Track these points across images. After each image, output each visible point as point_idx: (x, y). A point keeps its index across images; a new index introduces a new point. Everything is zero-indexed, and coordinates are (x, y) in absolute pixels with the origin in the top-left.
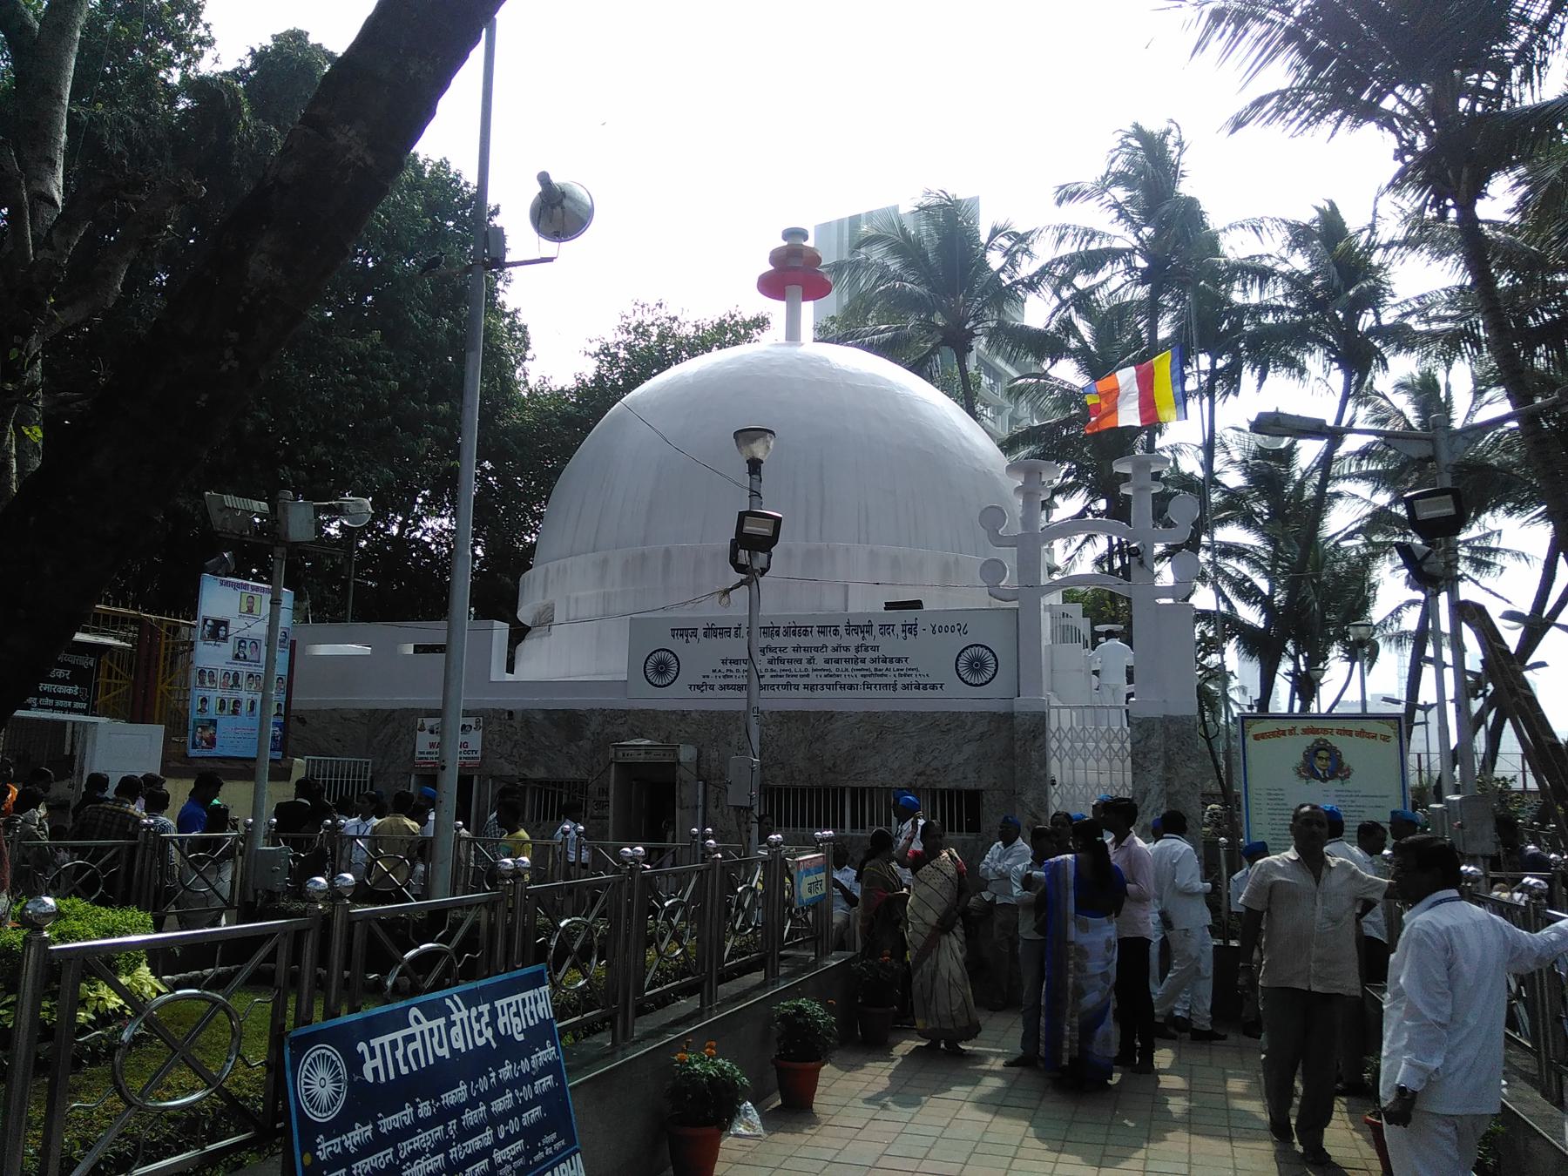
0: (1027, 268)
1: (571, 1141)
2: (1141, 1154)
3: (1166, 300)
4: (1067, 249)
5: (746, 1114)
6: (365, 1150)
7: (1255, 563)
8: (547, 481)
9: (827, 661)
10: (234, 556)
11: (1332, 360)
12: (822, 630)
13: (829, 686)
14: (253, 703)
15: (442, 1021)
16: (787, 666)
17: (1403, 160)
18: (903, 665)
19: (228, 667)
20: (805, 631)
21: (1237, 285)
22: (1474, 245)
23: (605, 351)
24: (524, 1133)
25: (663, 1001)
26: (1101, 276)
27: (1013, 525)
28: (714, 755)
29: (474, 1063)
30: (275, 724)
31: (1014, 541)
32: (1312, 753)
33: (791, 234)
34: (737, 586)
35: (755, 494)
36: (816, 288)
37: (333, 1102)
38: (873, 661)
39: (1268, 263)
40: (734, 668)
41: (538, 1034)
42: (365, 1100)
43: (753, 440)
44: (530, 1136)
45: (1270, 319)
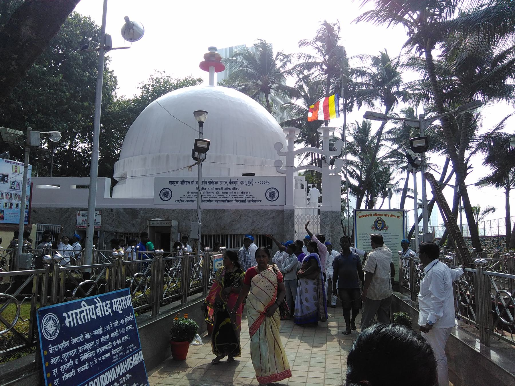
0: (289, 67)
1: (138, 347)
2: (325, 346)
3: (332, 80)
4: (302, 61)
5: (197, 338)
6: (67, 349)
7: (357, 166)
8: (123, 132)
9: (223, 193)
10: (10, 152)
11: (383, 102)
12: (221, 182)
13: (223, 201)
14: (17, 204)
15: (93, 306)
16: (209, 194)
17: (410, 36)
18: (248, 194)
19: (8, 191)
20: (216, 182)
21: (354, 76)
22: (429, 65)
23: (144, 87)
24: (122, 344)
25: (169, 302)
26: (312, 71)
27: (285, 149)
28: (184, 224)
29: (103, 321)
30: (26, 212)
31: (285, 154)
32: (376, 222)
33: (211, 49)
34: (194, 165)
35: (201, 133)
36: (219, 68)
37: (55, 333)
38: (238, 193)
39: (364, 69)
40: (191, 194)
41: (127, 311)
42: (66, 333)
43: (201, 115)
44: (125, 345)
45: (364, 88)
